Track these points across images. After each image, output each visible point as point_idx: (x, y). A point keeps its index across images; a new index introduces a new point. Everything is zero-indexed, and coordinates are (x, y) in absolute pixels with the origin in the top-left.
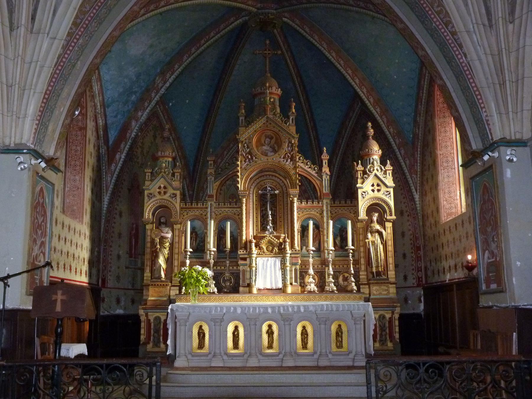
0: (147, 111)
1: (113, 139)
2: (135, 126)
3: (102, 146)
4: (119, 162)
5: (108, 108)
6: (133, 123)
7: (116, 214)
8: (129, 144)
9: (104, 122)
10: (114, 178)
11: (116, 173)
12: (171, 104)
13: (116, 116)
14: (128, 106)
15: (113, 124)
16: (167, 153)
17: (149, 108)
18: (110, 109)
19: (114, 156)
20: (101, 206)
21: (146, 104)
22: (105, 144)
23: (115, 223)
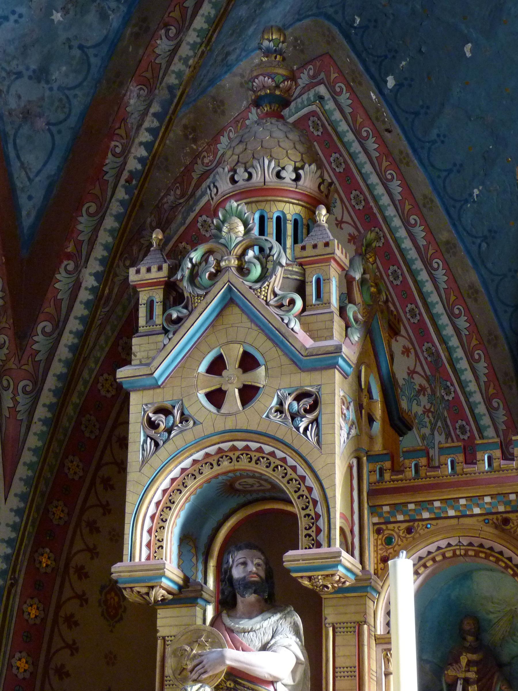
1: (39, 195)
4: (70, 308)
6: (133, 98)
7: (82, 599)
8: (115, 208)
10: (47, 397)
11: (57, 368)
12: (391, 82)
13: (41, 75)
14: (103, 16)
23: (73, 648)
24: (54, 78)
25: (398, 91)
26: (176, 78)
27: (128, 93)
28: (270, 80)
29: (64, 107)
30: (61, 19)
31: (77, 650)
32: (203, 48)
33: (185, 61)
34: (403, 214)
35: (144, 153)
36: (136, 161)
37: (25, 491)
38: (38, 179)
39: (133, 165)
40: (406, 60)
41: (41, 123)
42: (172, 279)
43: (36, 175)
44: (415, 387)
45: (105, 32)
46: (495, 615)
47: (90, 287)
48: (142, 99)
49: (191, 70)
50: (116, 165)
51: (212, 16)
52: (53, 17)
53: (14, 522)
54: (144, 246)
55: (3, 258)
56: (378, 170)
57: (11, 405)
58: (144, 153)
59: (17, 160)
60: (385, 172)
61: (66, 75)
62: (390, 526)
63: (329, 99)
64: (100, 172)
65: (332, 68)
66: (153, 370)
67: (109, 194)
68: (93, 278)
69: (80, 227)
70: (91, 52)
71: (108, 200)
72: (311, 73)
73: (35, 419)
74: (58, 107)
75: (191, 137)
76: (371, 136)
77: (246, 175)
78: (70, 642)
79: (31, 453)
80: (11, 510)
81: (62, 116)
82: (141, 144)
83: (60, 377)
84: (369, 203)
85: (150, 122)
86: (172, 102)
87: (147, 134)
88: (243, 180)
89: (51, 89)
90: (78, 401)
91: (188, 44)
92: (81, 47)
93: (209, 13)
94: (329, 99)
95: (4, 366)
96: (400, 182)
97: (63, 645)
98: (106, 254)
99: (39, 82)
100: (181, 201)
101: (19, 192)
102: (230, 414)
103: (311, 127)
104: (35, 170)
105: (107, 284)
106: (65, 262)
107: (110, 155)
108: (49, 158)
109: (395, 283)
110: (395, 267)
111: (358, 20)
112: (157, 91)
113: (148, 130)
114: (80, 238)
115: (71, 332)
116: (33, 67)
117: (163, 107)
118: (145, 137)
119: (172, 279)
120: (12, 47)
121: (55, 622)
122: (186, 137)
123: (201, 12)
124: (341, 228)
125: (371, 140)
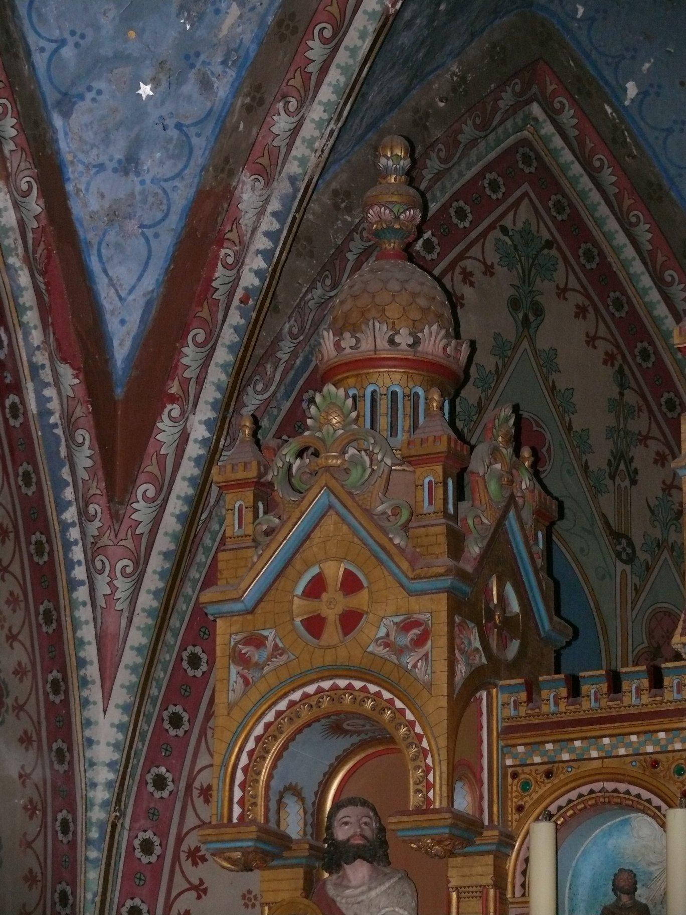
0: (326, 94)
1: (134, 318)
2: (259, 211)
3: (35, 369)
5: (66, 115)
6: (248, 193)
9: (35, 205)
11: (163, 543)
12: (632, 89)
13: (129, 164)
14: (206, 85)
15: (115, 216)
16: (373, 339)
17: (334, 76)
18: (81, 115)
19: (145, 430)
20: (69, 777)
21: (316, 50)
22: (61, 352)
24: (145, 168)
25: (642, 102)
26: (299, 166)
27: (241, 186)
28: (387, 211)
29: (161, 204)
30: (151, 93)
31: (205, 891)
32: (332, 126)
33: (310, 143)
34: (654, 267)
35: (263, 265)
36: (253, 275)
37: (128, 701)
38: (131, 297)
39: (249, 280)
40: (649, 61)
41: (132, 226)
42: (262, 480)
43: (131, 291)
44: (673, 507)
45: (209, 104)
46: (656, 867)
47: (200, 438)
48: (257, 193)
49: (317, 155)
50: (227, 280)
51: (342, 85)
52: (140, 92)
53: (116, 739)
54: (282, 361)
55: (90, 406)
56: (618, 211)
57: (109, 592)
58: (263, 265)
59: (103, 275)
60: (628, 215)
61: (162, 163)
62: (527, 769)
63: (545, 121)
64: (208, 289)
65: (548, 79)
66: (240, 592)
67: (220, 317)
68: (203, 427)
69: (185, 361)
70: (192, 131)
71: (219, 326)
72: (518, 88)
73: (138, 610)
74: (153, 204)
75: (343, 206)
76: (606, 167)
77: (354, 340)
78: (197, 882)
79: (135, 653)
80: (112, 725)
81: (159, 216)
82: (258, 252)
83: (166, 555)
84: (606, 258)
85: (269, 224)
86: (294, 197)
87: (265, 239)
88: (351, 347)
89: (142, 182)
90: (197, 576)
91: (313, 121)
92: (179, 126)
93: (338, 81)
94: (545, 121)
95: (97, 543)
96: (648, 226)
97: (188, 886)
98: (219, 396)
99: (126, 173)
100: (332, 294)
101: (108, 317)
102: (329, 647)
103: (520, 163)
104: (127, 287)
105: (222, 434)
106: (169, 407)
107: (219, 265)
108: (144, 271)
109: (644, 365)
110: (645, 344)
111: (581, 11)
112: (275, 183)
113: (267, 234)
114: (186, 375)
115: (178, 497)
116: (118, 156)
117: (284, 205)
118: (262, 243)
119: (262, 480)
120: (90, 133)
121: (176, 858)
122: (336, 207)
123: (327, 80)
124: (565, 299)
125: (607, 171)
